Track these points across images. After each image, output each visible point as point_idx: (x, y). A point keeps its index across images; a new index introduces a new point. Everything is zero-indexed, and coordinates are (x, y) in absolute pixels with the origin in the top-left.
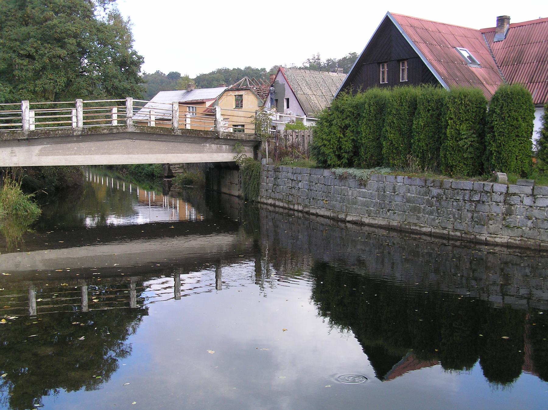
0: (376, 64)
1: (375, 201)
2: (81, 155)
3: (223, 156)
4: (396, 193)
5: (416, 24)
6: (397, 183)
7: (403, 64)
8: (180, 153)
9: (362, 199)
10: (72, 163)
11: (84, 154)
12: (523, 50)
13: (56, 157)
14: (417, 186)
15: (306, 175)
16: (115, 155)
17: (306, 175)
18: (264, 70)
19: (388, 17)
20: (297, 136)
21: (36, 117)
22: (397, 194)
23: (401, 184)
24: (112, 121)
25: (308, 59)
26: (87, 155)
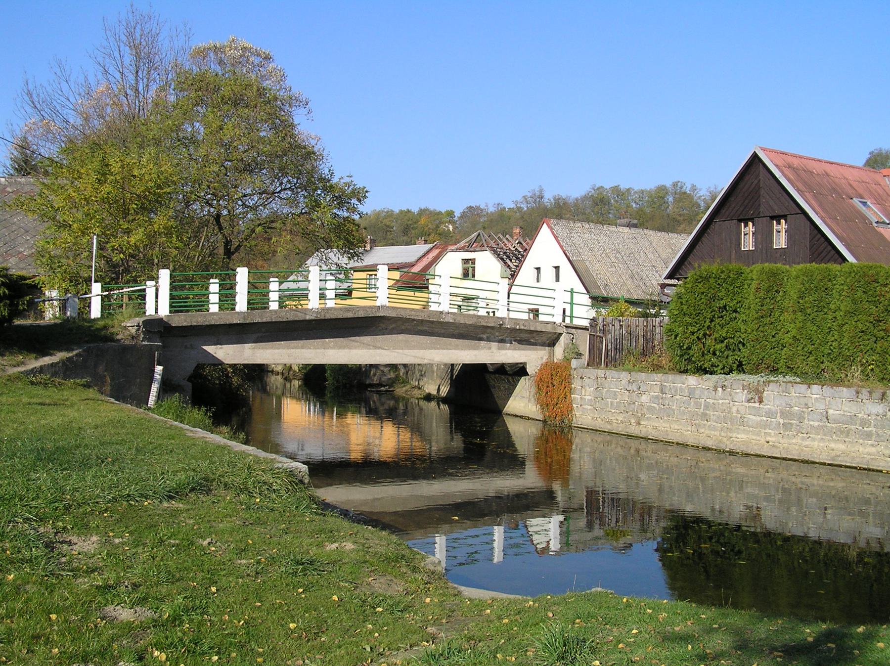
0: (735, 221)
1: (775, 420)
2: (310, 348)
3: (506, 354)
4: (810, 409)
5: (796, 162)
6: (811, 396)
7: (779, 223)
8: (447, 349)
9: (754, 418)
10: (323, 361)
11: (315, 348)
12: (830, 184)
13: (276, 351)
14: (844, 400)
15: (655, 383)
16: (357, 350)
17: (655, 383)
18: (450, 214)
19: (756, 154)
20: (621, 326)
21: (144, 287)
22: (812, 410)
23: (818, 396)
24: (91, 297)
25: (524, 197)
26: (319, 349)
